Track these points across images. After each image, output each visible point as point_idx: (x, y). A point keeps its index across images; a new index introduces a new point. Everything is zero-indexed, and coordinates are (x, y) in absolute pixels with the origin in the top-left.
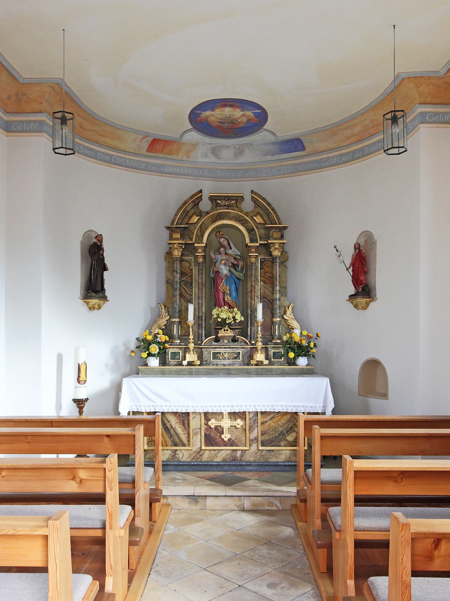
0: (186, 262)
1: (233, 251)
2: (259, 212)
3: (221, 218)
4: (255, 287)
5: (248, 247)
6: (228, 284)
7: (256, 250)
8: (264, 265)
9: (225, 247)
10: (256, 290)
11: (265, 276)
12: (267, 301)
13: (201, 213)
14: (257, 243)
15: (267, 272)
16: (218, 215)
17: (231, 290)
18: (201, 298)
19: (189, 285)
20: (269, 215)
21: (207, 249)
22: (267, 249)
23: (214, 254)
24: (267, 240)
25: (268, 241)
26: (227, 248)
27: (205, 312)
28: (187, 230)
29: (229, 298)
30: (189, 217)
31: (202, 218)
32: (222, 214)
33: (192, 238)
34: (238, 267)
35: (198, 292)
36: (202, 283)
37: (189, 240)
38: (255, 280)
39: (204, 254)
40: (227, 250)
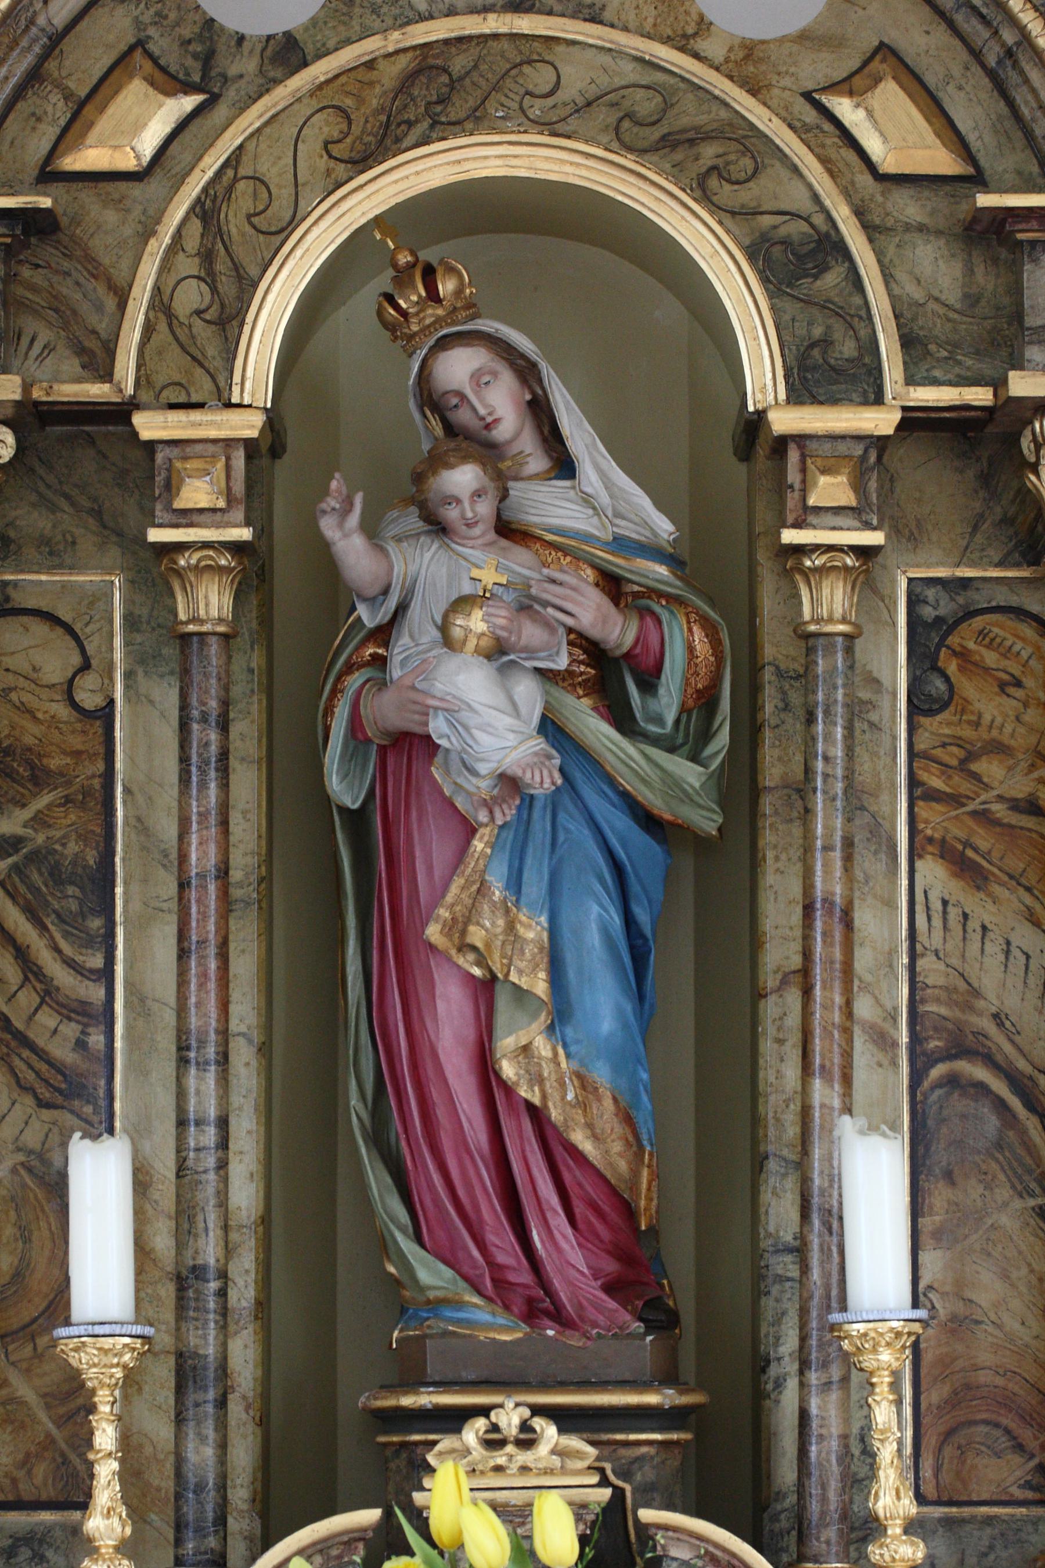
0: (40, 629)
1: (587, 500)
2: (895, 37)
3: (457, 109)
4: (848, 924)
5: (762, 451)
6: (535, 885)
7: (858, 486)
8: (952, 668)
9: (492, 446)
10: (864, 960)
11: (965, 787)
12: (1000, 1087)
13: (207, 59)
14: (878, 400)
15: (998, 748)
16: (410, 78)
17: (569, 957)
18: (211, 1052)
19: (72, 895)
20: (1012, 77)
21: (283, 470)
22: (985, 479)
23: (371, 529)
24: (987, 369)
25: (999, 384)
26: (520, 459)
27: (265, 1220)
28: (48, 253)
29: (543, 1047)
30: (68, 96)
31: (221, 111)
32: (459, 63)
33: (110, 351)
34: (649, 683)
35: (182, 982)
36: (223, 872)
37: (72, 365)
38: (848, 843)
39: (245, 534)
40: (516, 489)
